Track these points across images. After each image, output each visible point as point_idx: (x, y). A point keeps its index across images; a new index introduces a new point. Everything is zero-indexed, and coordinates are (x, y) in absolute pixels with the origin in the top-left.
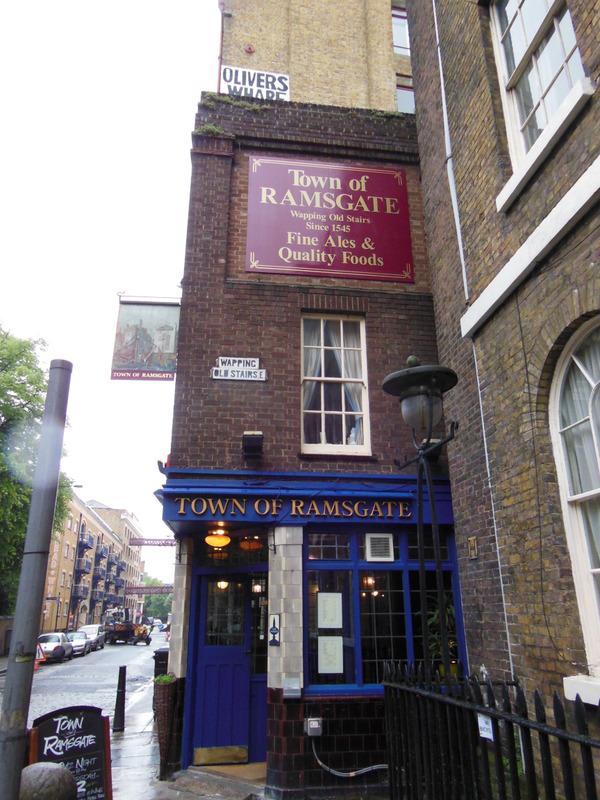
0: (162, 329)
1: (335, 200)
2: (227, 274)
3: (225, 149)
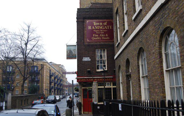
0: (74, 50)
2: (84, 42)
3: (82, 20)
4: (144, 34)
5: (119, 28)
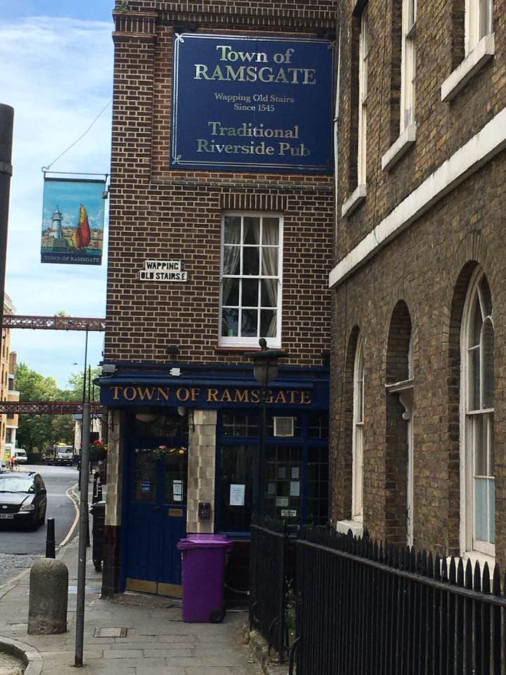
1: (257, 73)
4: (494, 196)
5: (365, 105)
